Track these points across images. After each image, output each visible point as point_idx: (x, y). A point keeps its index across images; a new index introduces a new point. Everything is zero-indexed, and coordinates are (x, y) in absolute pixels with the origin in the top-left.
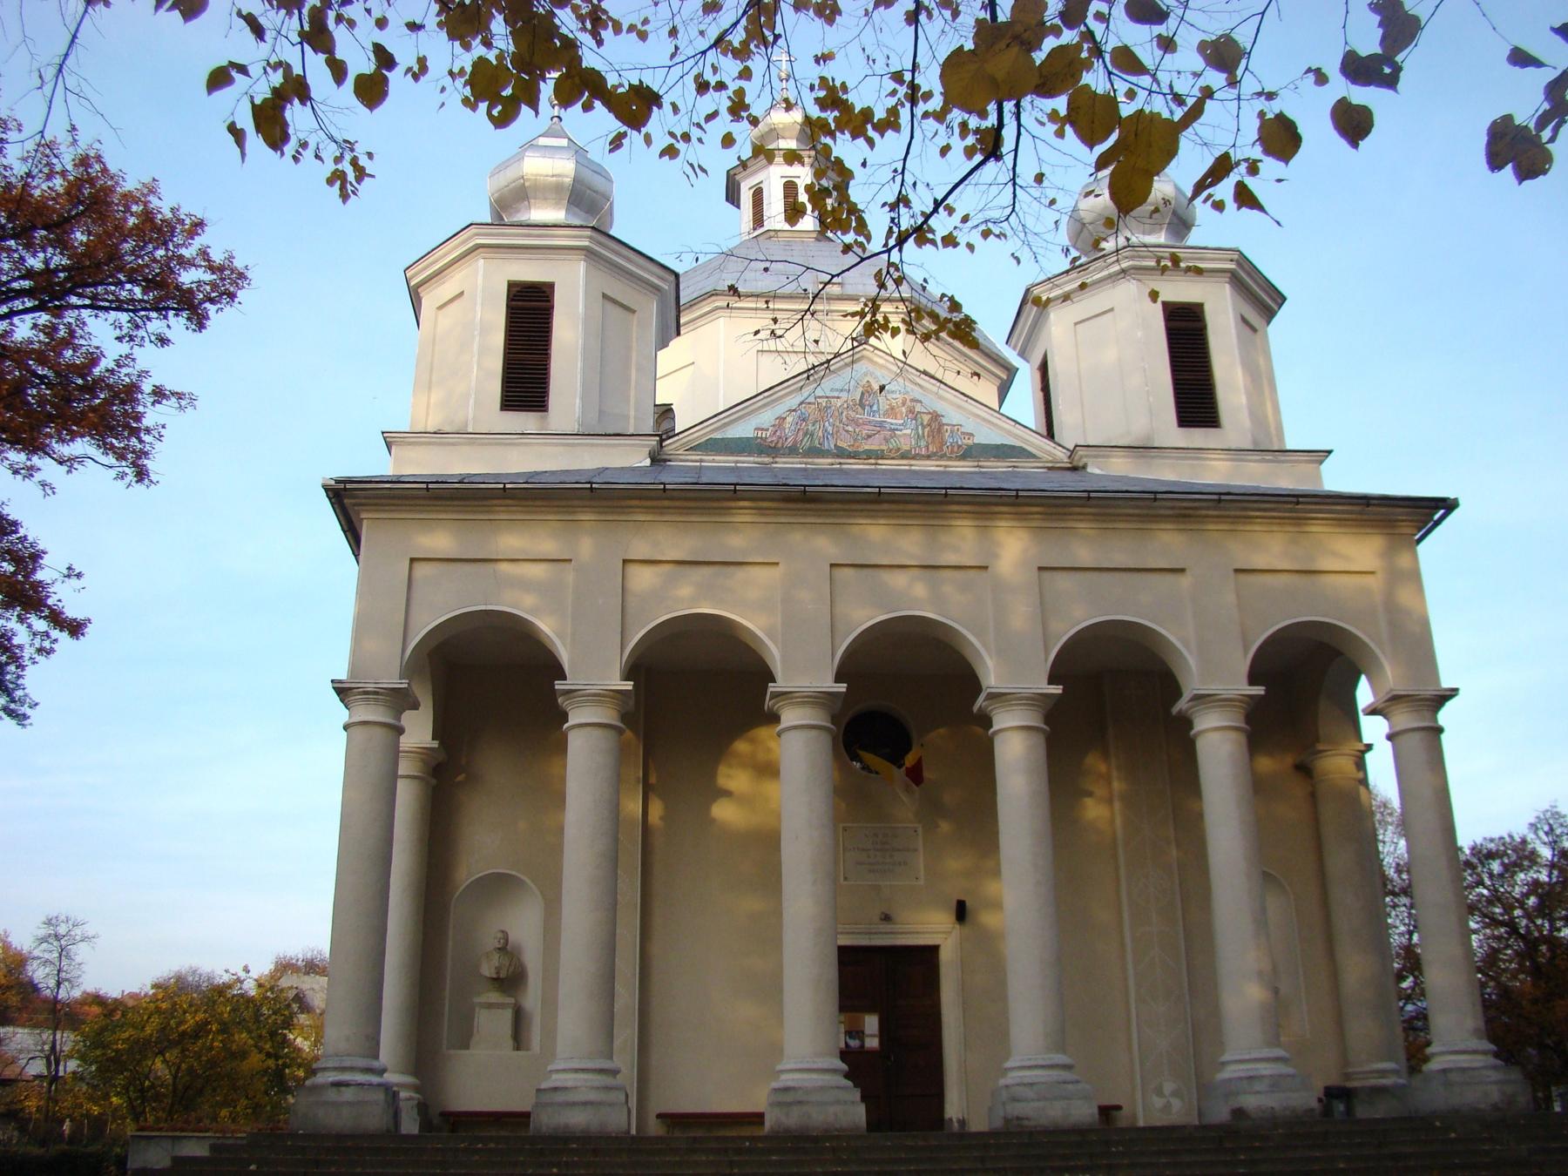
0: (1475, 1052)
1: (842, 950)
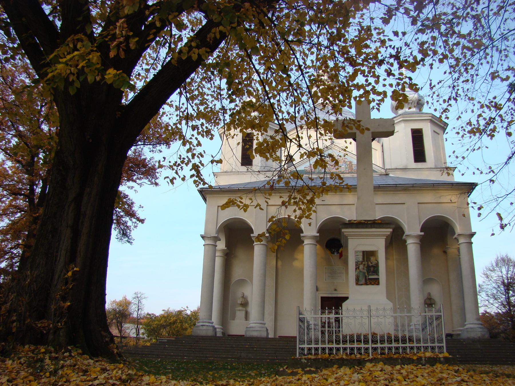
0: (475, 324)
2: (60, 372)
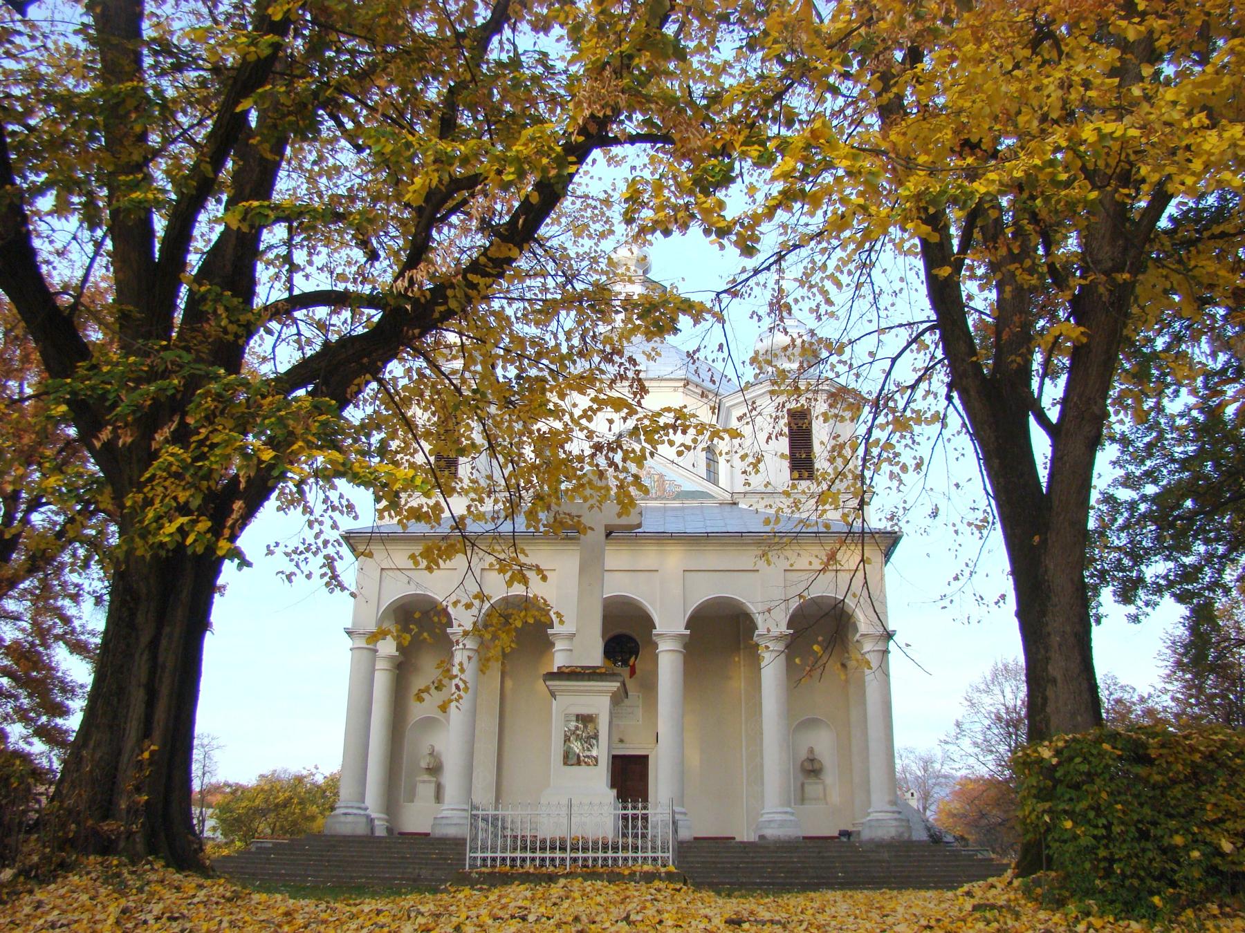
1: (615, 757)
2: (147, 888)
